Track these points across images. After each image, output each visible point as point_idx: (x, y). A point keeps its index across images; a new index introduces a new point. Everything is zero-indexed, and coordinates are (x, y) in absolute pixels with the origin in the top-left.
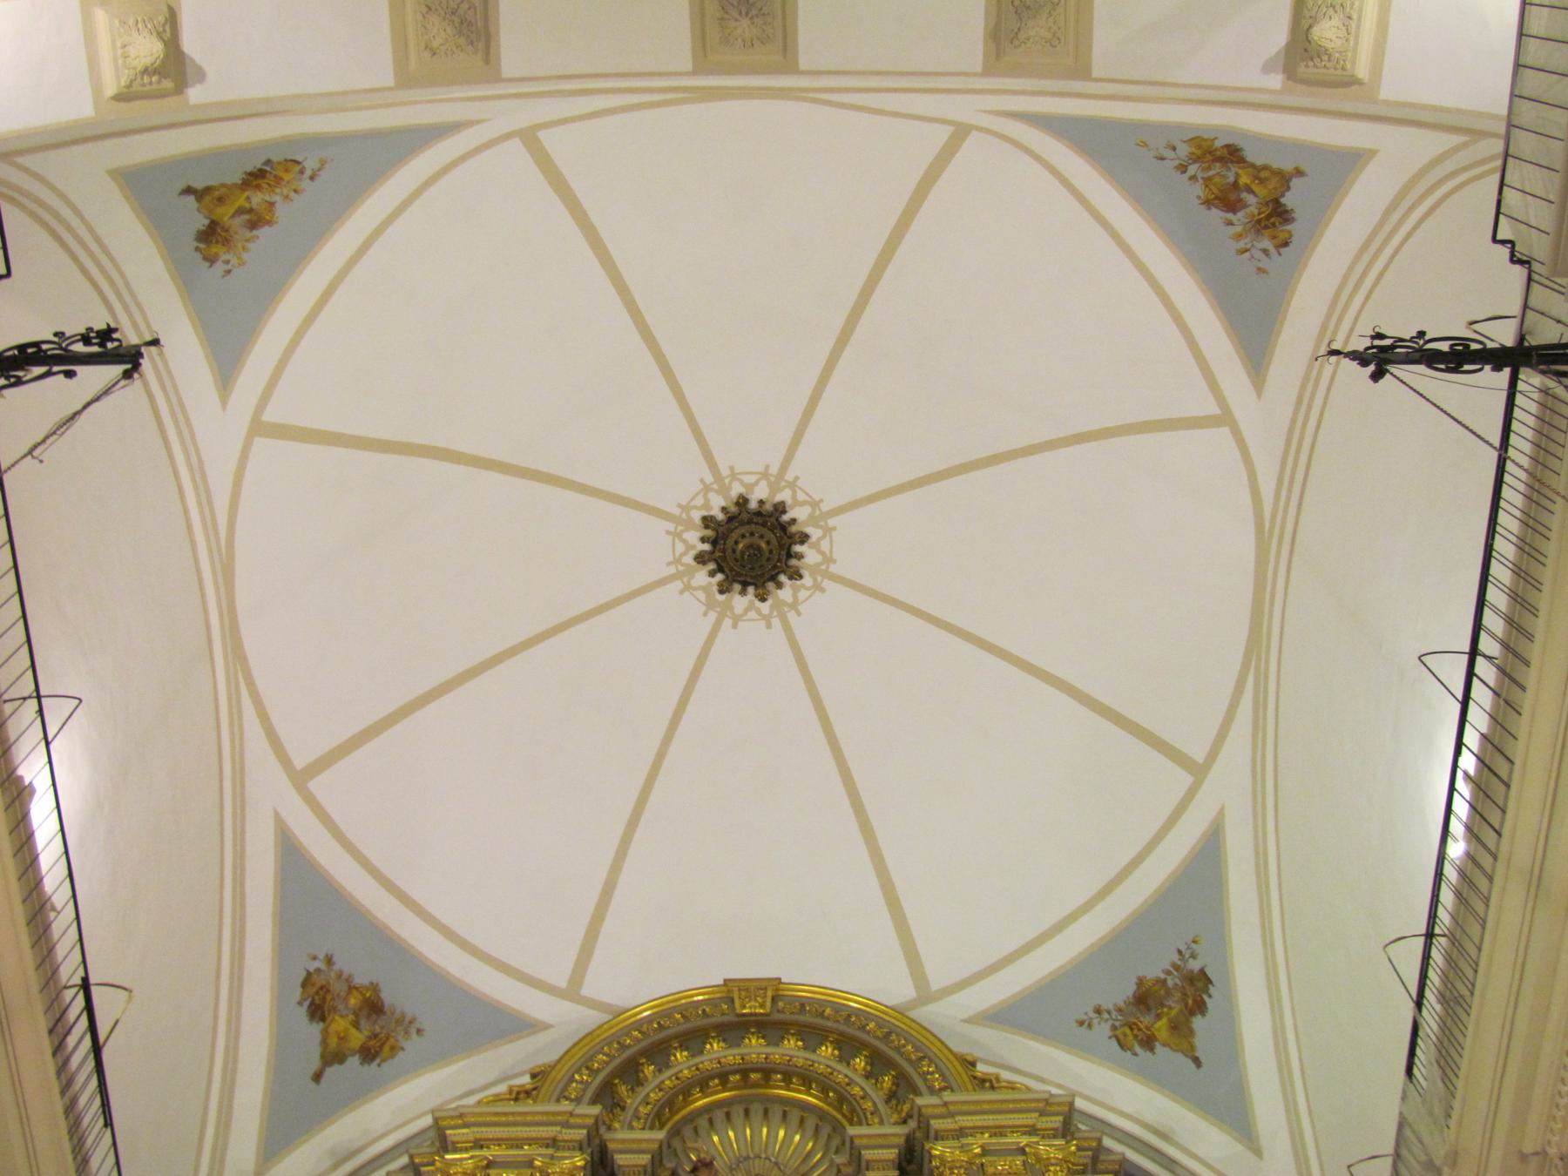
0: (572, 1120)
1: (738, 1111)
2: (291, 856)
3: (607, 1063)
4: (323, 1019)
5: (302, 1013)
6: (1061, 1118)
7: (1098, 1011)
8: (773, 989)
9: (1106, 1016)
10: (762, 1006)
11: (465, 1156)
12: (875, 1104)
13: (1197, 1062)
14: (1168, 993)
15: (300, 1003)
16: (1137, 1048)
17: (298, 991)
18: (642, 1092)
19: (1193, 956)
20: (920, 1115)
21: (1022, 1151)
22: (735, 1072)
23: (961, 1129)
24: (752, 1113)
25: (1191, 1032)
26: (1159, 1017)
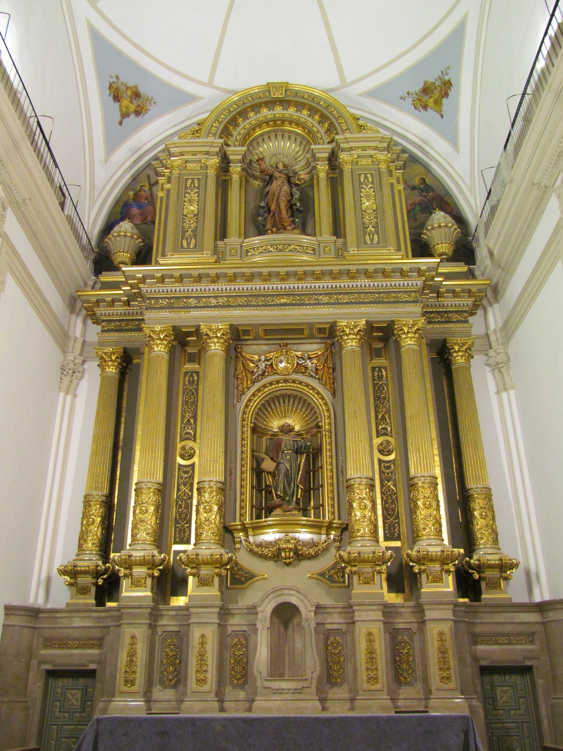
0: (214, 144)
1: (273, 135)
2: (96, 36)
3: (225, 119)
4: (119, 101)
5: (111, 99)
6: (387, 144)
7: (408, 94)
8: (285, 86)
9: (411, 96)
10: (281, 94)
11: (177, 158)
12: (321, 135)
13: (442, 116)
14: (436, 88)
15: (109, 96)
16: (421, 109)
17: (108, 92)
18: (239, 129)
19: (447, 74)
20: (337, 142)
21: (372, 156)
22: (271, 121)
23: (351, 147)
24: (278, 136)
25: (441, 104)
26: (430, 97)
